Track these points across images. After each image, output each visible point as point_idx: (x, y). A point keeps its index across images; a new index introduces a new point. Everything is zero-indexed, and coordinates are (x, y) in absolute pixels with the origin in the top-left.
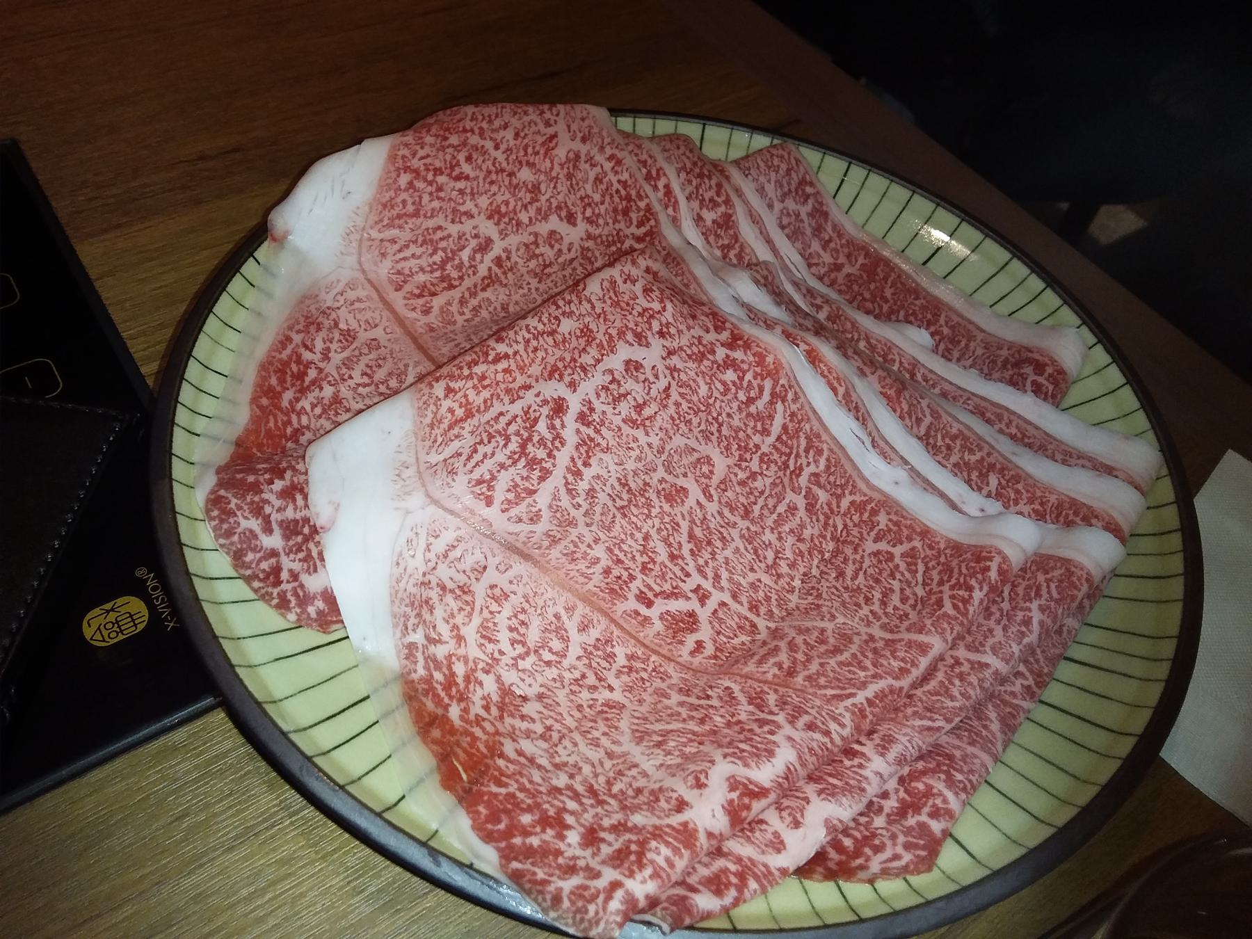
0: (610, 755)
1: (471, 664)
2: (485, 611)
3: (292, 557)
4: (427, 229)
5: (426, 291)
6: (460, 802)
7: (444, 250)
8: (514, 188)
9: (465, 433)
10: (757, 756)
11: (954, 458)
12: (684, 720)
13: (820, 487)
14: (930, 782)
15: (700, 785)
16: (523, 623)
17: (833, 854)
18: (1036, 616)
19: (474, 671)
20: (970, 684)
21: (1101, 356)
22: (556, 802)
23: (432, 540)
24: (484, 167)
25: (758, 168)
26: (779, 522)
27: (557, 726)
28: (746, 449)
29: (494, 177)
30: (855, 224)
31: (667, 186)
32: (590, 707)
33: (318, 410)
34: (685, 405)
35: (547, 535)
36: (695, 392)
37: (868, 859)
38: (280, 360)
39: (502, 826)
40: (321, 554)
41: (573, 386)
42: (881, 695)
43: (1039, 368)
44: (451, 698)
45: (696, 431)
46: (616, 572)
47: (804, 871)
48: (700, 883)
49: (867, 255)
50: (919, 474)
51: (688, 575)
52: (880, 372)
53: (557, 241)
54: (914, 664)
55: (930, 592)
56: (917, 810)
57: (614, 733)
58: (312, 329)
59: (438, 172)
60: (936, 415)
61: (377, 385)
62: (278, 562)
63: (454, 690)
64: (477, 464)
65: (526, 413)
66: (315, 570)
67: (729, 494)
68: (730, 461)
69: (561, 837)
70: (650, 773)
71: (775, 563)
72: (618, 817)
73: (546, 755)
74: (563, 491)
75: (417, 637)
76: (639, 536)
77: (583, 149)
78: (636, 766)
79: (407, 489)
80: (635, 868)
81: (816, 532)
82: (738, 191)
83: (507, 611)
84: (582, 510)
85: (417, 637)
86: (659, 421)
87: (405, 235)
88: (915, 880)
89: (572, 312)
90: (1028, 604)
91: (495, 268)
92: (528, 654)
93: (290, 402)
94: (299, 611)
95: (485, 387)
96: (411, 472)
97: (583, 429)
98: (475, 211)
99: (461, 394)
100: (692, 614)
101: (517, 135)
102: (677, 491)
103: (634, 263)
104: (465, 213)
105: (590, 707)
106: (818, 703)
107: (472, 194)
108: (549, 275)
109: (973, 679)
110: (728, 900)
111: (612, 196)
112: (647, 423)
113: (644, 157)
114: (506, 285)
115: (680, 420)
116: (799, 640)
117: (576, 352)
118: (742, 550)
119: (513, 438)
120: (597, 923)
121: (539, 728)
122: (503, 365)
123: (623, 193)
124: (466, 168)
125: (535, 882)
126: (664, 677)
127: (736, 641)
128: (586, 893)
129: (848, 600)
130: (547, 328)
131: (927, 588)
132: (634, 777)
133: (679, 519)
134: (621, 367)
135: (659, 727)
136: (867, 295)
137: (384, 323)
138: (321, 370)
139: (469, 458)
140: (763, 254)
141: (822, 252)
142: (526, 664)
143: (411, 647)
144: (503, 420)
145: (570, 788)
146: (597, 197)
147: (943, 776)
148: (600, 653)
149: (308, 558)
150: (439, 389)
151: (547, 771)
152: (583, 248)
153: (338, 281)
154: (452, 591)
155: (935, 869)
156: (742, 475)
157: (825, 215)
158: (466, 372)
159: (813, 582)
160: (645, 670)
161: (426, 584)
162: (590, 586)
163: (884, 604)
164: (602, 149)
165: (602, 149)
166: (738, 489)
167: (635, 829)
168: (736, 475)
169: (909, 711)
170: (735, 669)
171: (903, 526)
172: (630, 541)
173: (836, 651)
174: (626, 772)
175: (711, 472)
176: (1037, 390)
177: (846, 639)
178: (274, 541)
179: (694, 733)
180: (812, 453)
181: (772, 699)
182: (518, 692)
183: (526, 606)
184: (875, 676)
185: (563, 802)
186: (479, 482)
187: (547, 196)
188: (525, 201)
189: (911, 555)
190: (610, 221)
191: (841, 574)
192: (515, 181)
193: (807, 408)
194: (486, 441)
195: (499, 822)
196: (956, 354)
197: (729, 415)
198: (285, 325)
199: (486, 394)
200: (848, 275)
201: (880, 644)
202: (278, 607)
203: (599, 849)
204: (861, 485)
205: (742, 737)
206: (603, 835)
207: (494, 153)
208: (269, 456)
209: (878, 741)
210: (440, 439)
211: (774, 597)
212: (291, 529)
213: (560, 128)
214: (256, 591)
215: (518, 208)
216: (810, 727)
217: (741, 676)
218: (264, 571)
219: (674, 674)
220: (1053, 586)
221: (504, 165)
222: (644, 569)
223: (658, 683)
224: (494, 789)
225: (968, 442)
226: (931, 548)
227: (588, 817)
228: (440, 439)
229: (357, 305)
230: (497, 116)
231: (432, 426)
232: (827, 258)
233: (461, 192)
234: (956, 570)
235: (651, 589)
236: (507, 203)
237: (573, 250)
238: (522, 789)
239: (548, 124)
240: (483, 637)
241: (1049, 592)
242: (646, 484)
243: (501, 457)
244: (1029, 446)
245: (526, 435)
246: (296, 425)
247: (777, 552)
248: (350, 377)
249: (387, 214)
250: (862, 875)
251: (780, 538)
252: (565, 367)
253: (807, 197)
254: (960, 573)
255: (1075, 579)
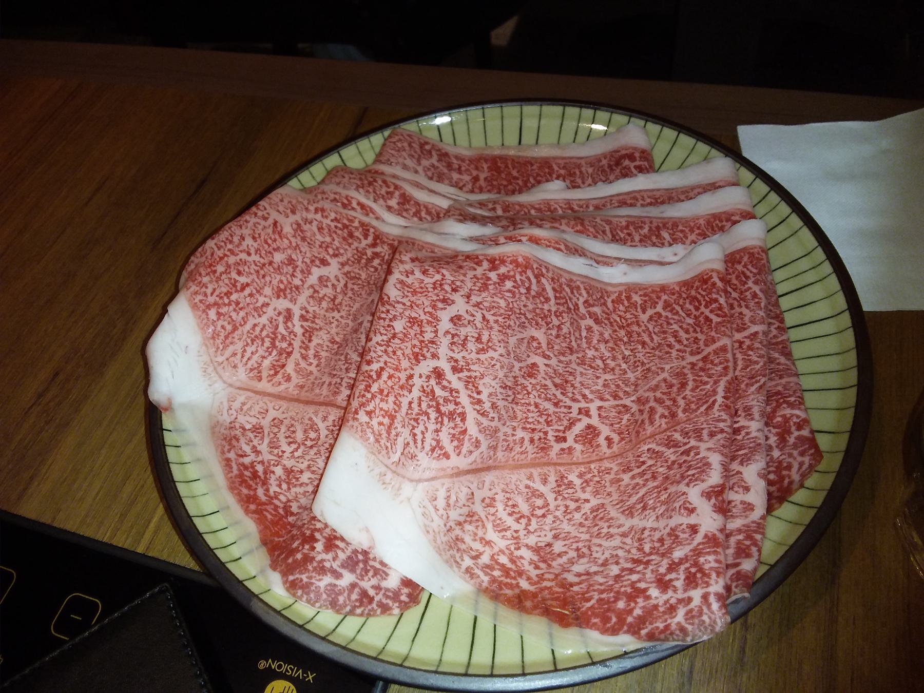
0: (624, 535)
1: (507, 552)
2: (489, 517)
3: (366, 578)
4: (248, 332)
5: (277, 368)
6: (581, 627)
7: (268, 336)
8: (278, 270)
9: (400, 429)
10: (703, 471)
11: (637, 238)
12: (644, 485)
13: (593, 306)
14: (782, 413)
15: (692, 511)
16: (514, 506)
17: (772, 489)
18: (756, 289)
19: (512, 554)
20: (758, 348)
21: (654, 128)
22: (625, 583)
23: (435, 503)
24: (252, 271)
25: (393, 155)
26: (589, 342)
27: (580, 545)
28: (546, 317)
29: (262, 272)
30: (465, 148)
31: (359, 204)
32: (586, 519)
33: (284, 486)
34: (500, 319)
35: (489, 447)
36: (499, 308)
37: (789, 477)
38: (236, 476)
39: (614, 620)
40: (382, 563)
41: (435, 356)
42: (727, 390)
43: (631, 157)
44: (515, 578)
45: (516, 328)
46: (536, 438)
47: (770, 509)
48: (735, 559)
49: (486, 161)
50: (631, 260)
51: (570, 408)
52: (564, 221)
53: (326, 281)
54: (727, 361)
55: (696, 317)
56: (789, 433)
57: (613, 522)
58: (234, 442)
59: (228, 294)
60: (609, 222)
61: (303, 444)
62: (360, 588)
63: (512, 573)
64: (423, 441)
65: (424, 391)
66: (387, 575)
67: (556, 347)
68: (543, 330)
69: (648, 598)
70: (656, 526)
71: (605, 365)
72: (665, 563)
73: (592, 564)
74: (479, 417)
75: (468, 562)
76: (532, 408)
77: (297, 217)
78: (644, 529)
79: (397, 486)
80: (707, 580)
81: (610, 331)
82: (394, 176)
83: (500, 506)
84: (497, 419)
85: (468, 562)
86: (495, 339)
87: (239, 346)
88: (820, 467)
89: (395, 316)
90: (747, 286)
91: (305, 324)
92: (529, 520)
93: (266, 495)
94: (397, 604)
95: (387, 396)
96: (389, 475)
97: (461, 375)
98: (267, 300)
99: (377, 411)
100: (589, 427)
101: (254, 238)
102: (532, 368)
103: (402, 262)
104: (263, 306)
105: (586, 519)
106: (702, 419)
107: (258, 292)
108: (341, 304)
109: (757, 345)
110: (756, 554)
111: (336, 232)
112: (490, 344)
113: (332, 196)
114: (321, 329)
115: (504, 329)
116: (658, 394)
117: (418, 336)
118: (584, 371)
119: (430, 411)
120: (715, 622)
121: (572, 554)
122: (385, 376)
123: (339, 225)
124: (243, 280)
125: (662, 632)
126: (608, 471)
127: (624, 422)
128: (694, 613)
129: (661, 354)
130: (390, 336)
131: (692, 316)
132: (650, 536)
133: (544, 382)
134: (451, 325)
135: (634, 499)
136: (505, 183)
137: (270, 406)
138: (262, 462)
139: (415, 441)
140: (444, 204)
141: (461, 177)
142: (534, 525)
143: (468, 570)
144: (415, 405)
145: (623, 570)
146: (328, 239)
147: (785, 405)
148: (563, 487)
149: (376, 572)
150: (363, 417)
151: (602, 572)
152: (345, 274)
153: (222, 403)
154: (465, 521)
155: (824, 454)
156: (554, 332)
157: (446, 155)
158: (369, 396)
159: (632, 359)
160: (595, 476)
161: (450, 530)
162: (530, 456)
163: (679, 342)
164: (307, 209)
165: (307, 209)
166: (558, 341)
167: (681, 561)
168: (551, 334)
169: (743, 386)
170: (642, 437)
171: (652, 294)
172: (530, 415)
173: (683, 385)
174: (643, 536)
175: (539, 343)
176: (641, 170)
177: (680, 374)
178: (348, 578)
179: (657, 487)
180: (575, 292)
181: (677, 436)
182: (543, 544)
183: (508, 495)
184: (716, 382)
185: (629, 580)
186: (433, 450)
187: (300, 260)
188: (290, 273)
189: (667, 305)
190: (347, 247)
191: (644, 344)
192: (276, 266)
193: (556, 270)
194: (416, 425)
195: (610, 619)
196: (579, 181)
197: (525, 306)
198: (219, 454)
199: (391, 399)
200: (485, 179)
201: (701, 364)
202: (383, 612)
203: (674, 586)
204: (610, 289)
205: (684, 468)
206: (667, 578)
207: (250, 259)
208: (292, 537)
209: (743, 414)
210: (389, 445)
211: (620, 383)
212: (351, 564)
213: (274, 215)
214: (362, 615)
215: (290, 279)
216: (712, 435)
217: (649, 437)
218: (356, 600)
219: (611, 466)
220: (750, 267)
221: (262, 261)
222: (548, 423)
223: (608, 478)
224: (589, 605)
225: (635, 224)
226: (673, 294)
227: (649, 575)
228: (389, 445)
229: (245, 408)
230: (232, 236)
231: (377, 441)
232: (466, 178)
233: (251, 295)
234: (699, 296)
235: (559, 431)
236: (281, 282)
237: (341, 279)
238: (602, 592)
239: (265, 219)
240: (499, 531)
241: (751, 272)
242: (515, 377)
243: (432, 427)
244: (663, 203)
245: (434, 403)
246: (282, 505)
247: (601, 358)
248: (283, 452)
249: (218, 341)
250: (795, 486)
251: (597, 350)
252: (420, 349)
253: (430, 152)
254: (703, 296)
255: (757, 255)
